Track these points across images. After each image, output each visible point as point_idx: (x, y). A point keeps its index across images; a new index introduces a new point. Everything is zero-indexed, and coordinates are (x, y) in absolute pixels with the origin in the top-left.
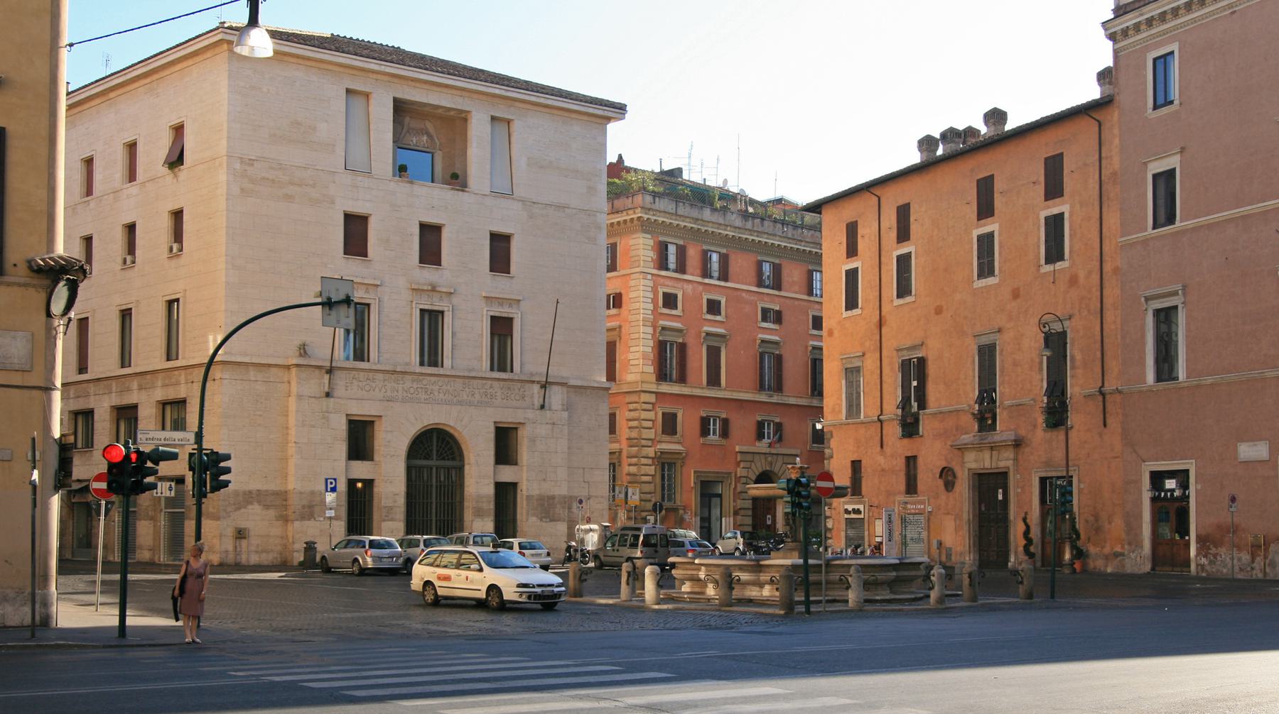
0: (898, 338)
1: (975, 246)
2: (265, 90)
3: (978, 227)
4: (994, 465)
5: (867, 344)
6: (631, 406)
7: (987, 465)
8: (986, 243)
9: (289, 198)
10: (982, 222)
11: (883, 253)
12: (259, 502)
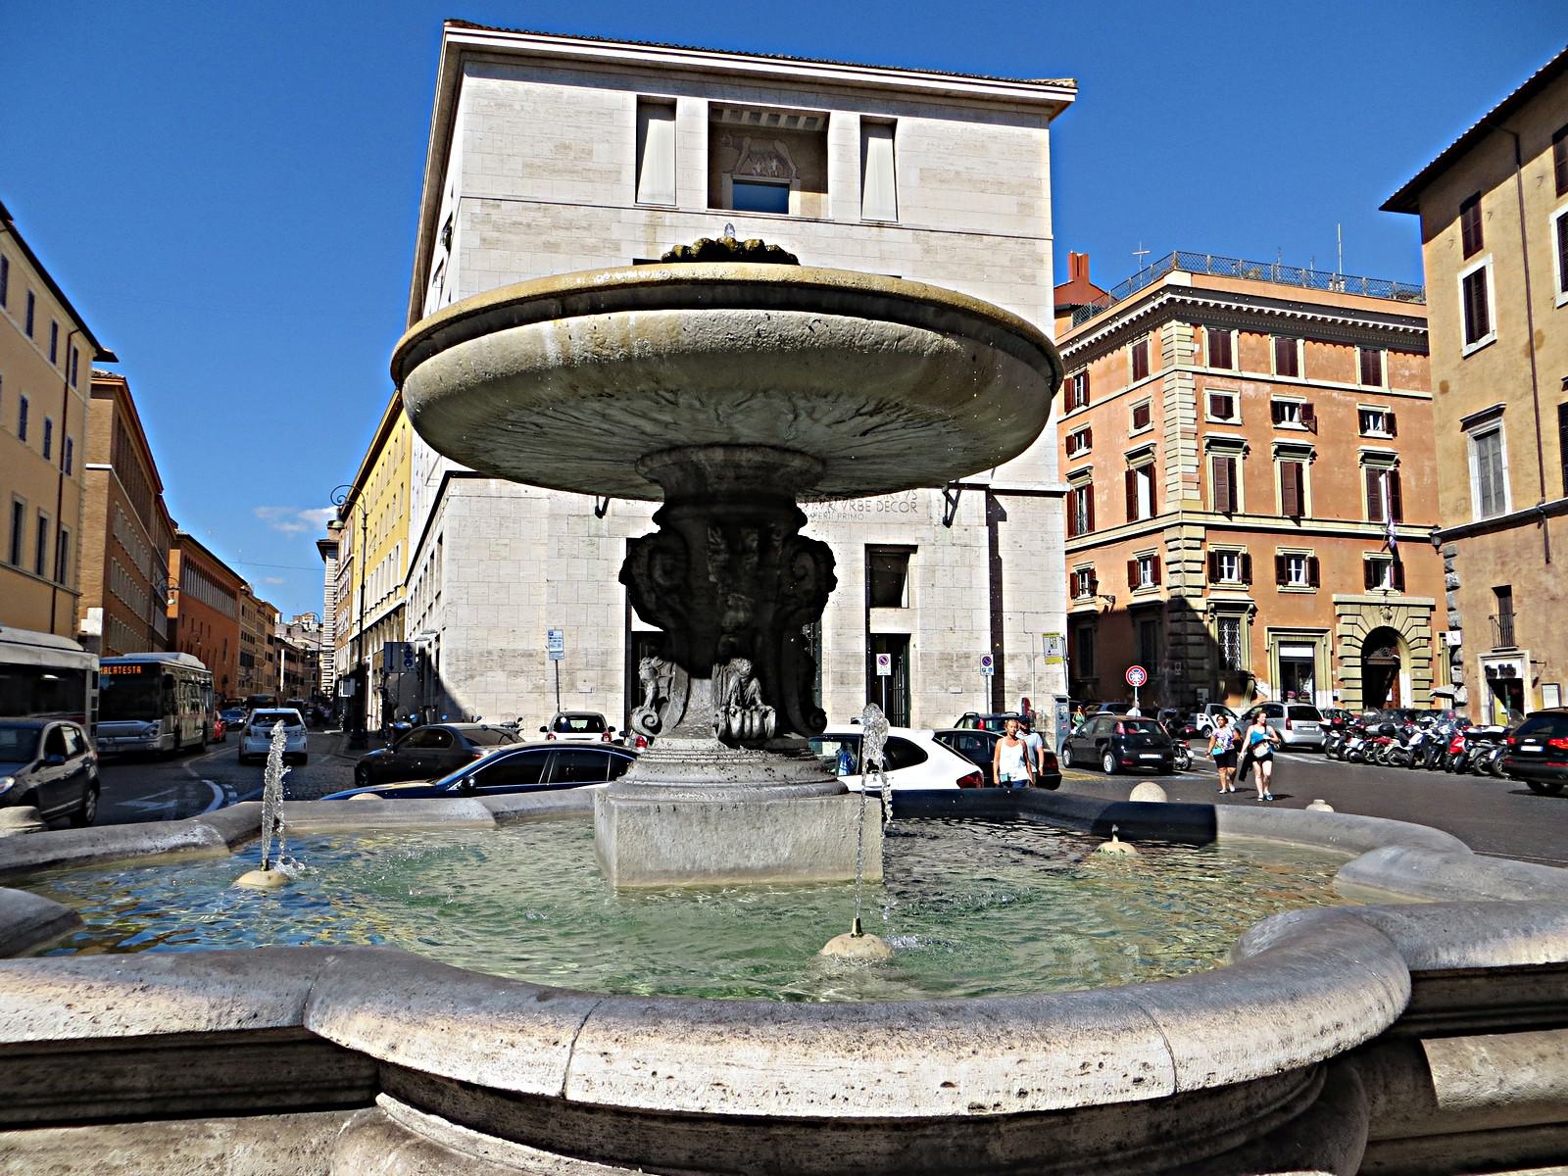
2: (517, 107)
6: (1171, 545)
9: (551, 247)
12: (503, 667)
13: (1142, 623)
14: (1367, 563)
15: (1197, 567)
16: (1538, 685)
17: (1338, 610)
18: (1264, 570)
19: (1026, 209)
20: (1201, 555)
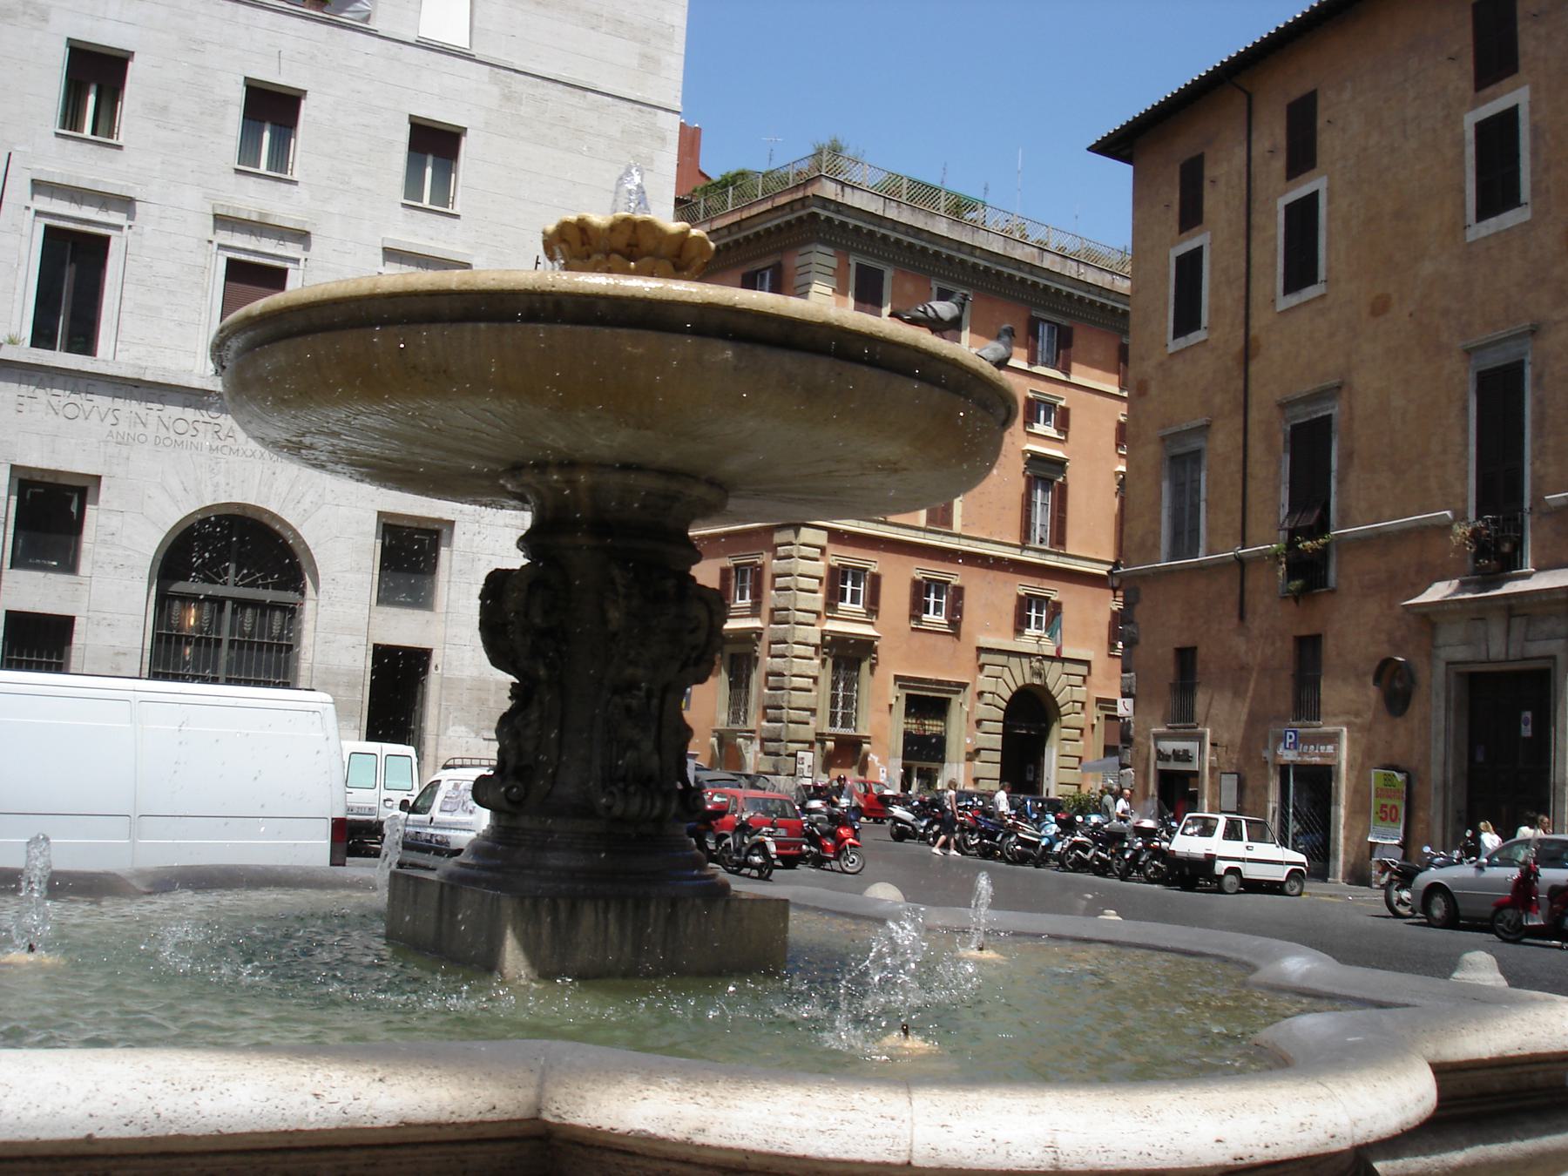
0: (1282, 374)
1: (1470, 150)
3: (1474, 107)
4: (1514, 652)
5: (1218, 400)
7: (1497, 649)
8: (1498, 137)
10: (1488, 91)
11: (1256, 206)
13: (733, 656)
14: (1020, 598)
15: (814, 584)
16: (1217, 774)
17: (984, 658)
18: (895, 596)
19: (649, 63)
20: (820, 568)
